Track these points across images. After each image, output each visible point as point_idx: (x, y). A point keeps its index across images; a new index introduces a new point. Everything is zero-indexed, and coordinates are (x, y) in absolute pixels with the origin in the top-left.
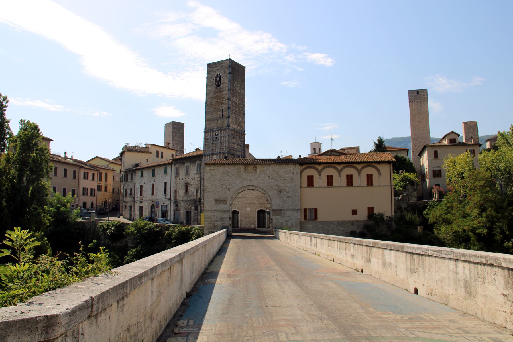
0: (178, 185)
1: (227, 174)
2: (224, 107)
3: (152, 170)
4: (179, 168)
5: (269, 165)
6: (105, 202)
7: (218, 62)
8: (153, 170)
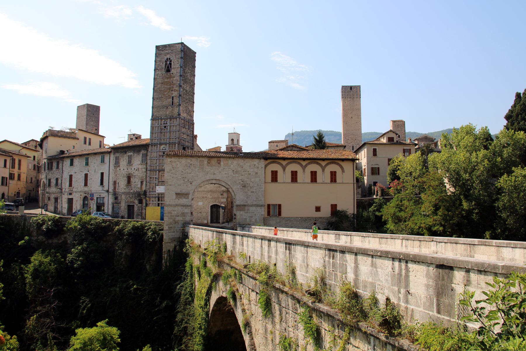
0: (118, 175)
1: (189, 167)
2: (175, 94)
3: (85, 159)
4: (120, 157)
5: (233, 158)
6: (17, 192)
7: (169, 45)
8: (86, 158)
